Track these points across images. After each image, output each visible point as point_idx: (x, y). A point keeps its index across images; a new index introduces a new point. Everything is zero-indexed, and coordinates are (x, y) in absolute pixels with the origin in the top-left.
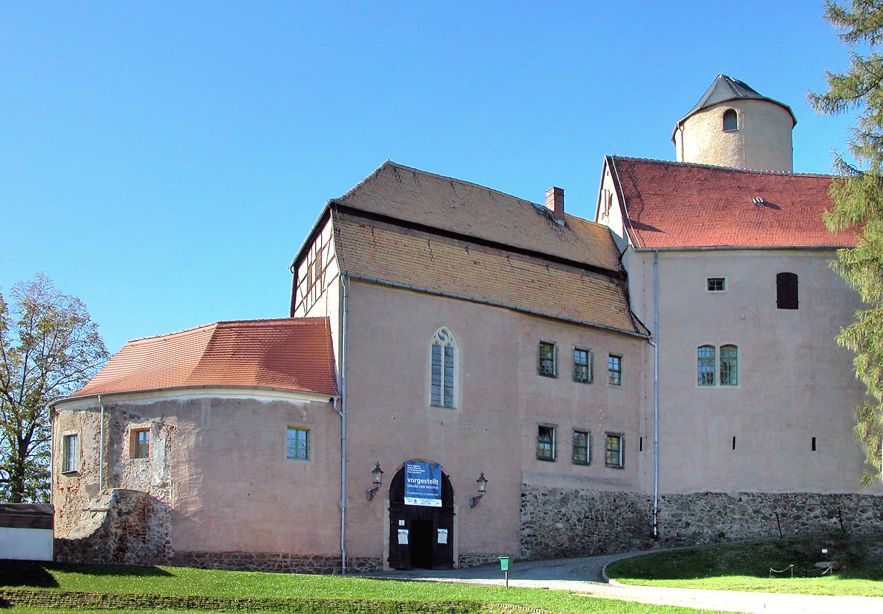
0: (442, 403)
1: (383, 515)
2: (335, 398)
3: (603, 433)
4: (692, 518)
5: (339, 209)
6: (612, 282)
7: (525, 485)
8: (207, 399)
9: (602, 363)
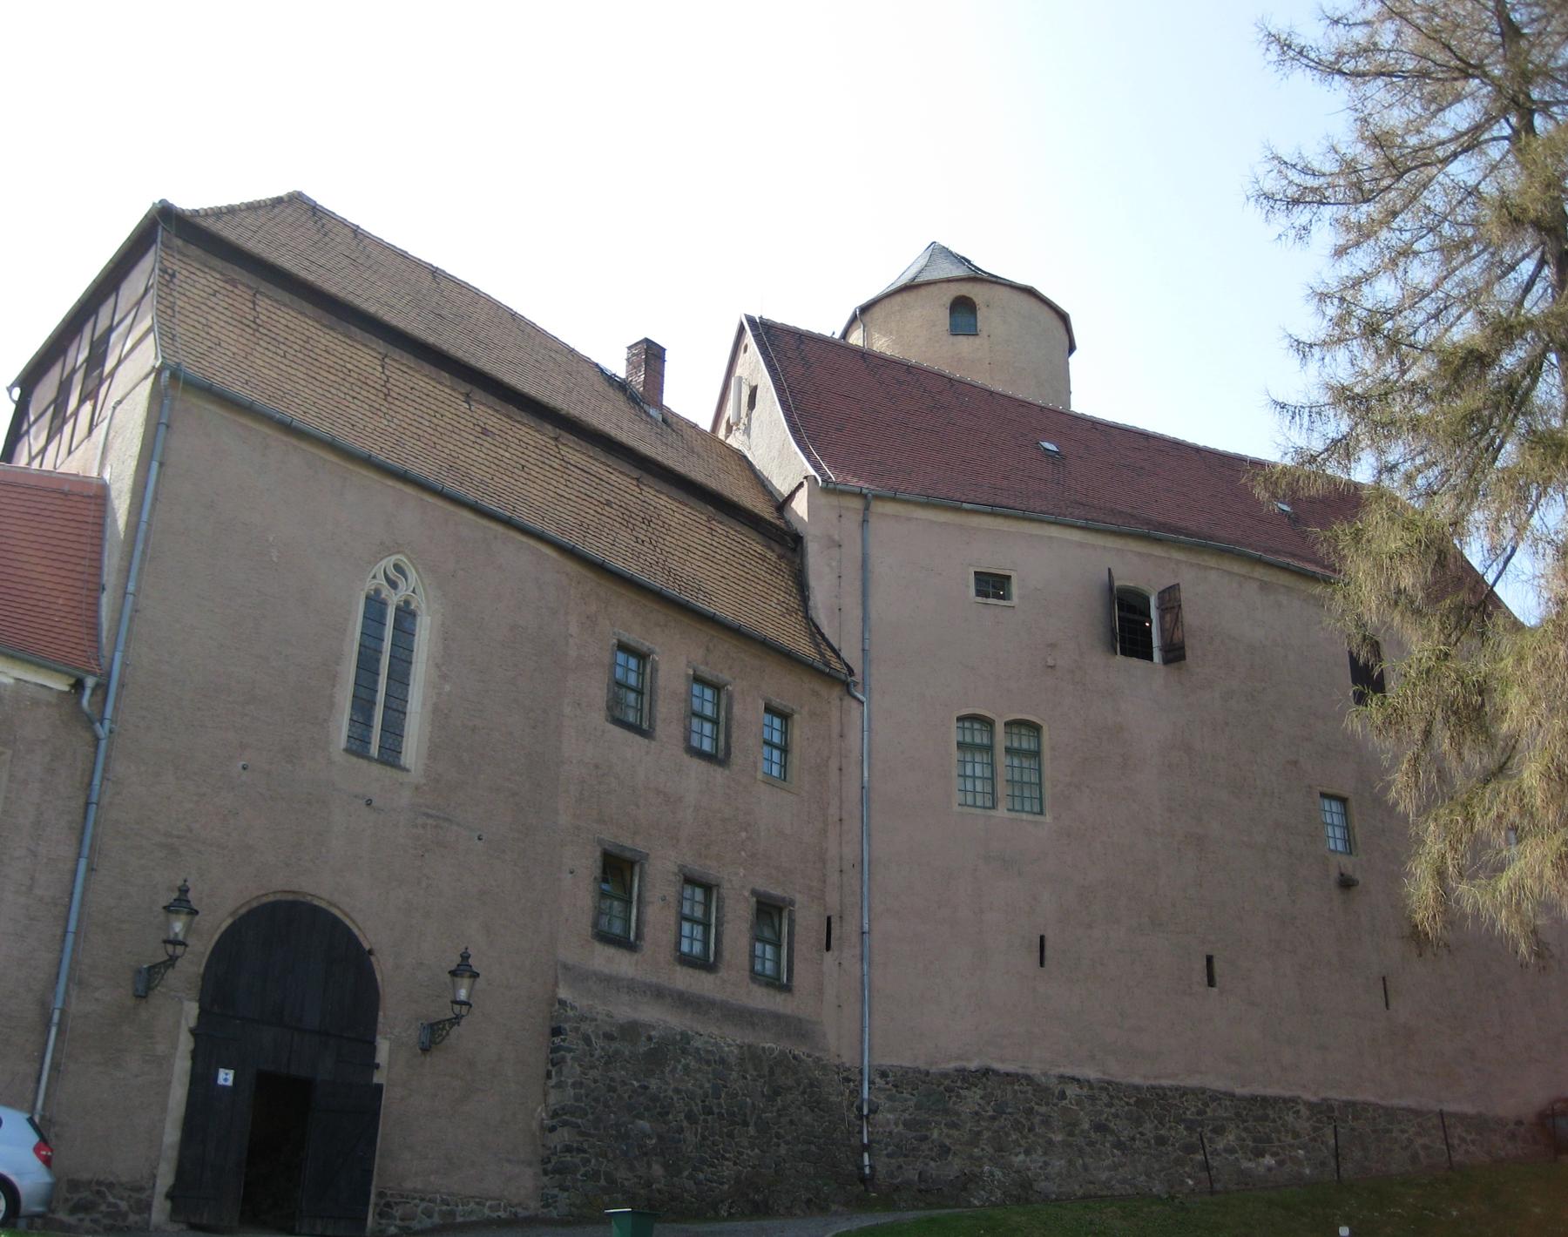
0: (374, 750)
1: (175, 1047)
2: (90, 682)
3: (747, 894)
4: (955, 1133)
6: (769, 548)
7: (562, 1003)
9: (749, 715)
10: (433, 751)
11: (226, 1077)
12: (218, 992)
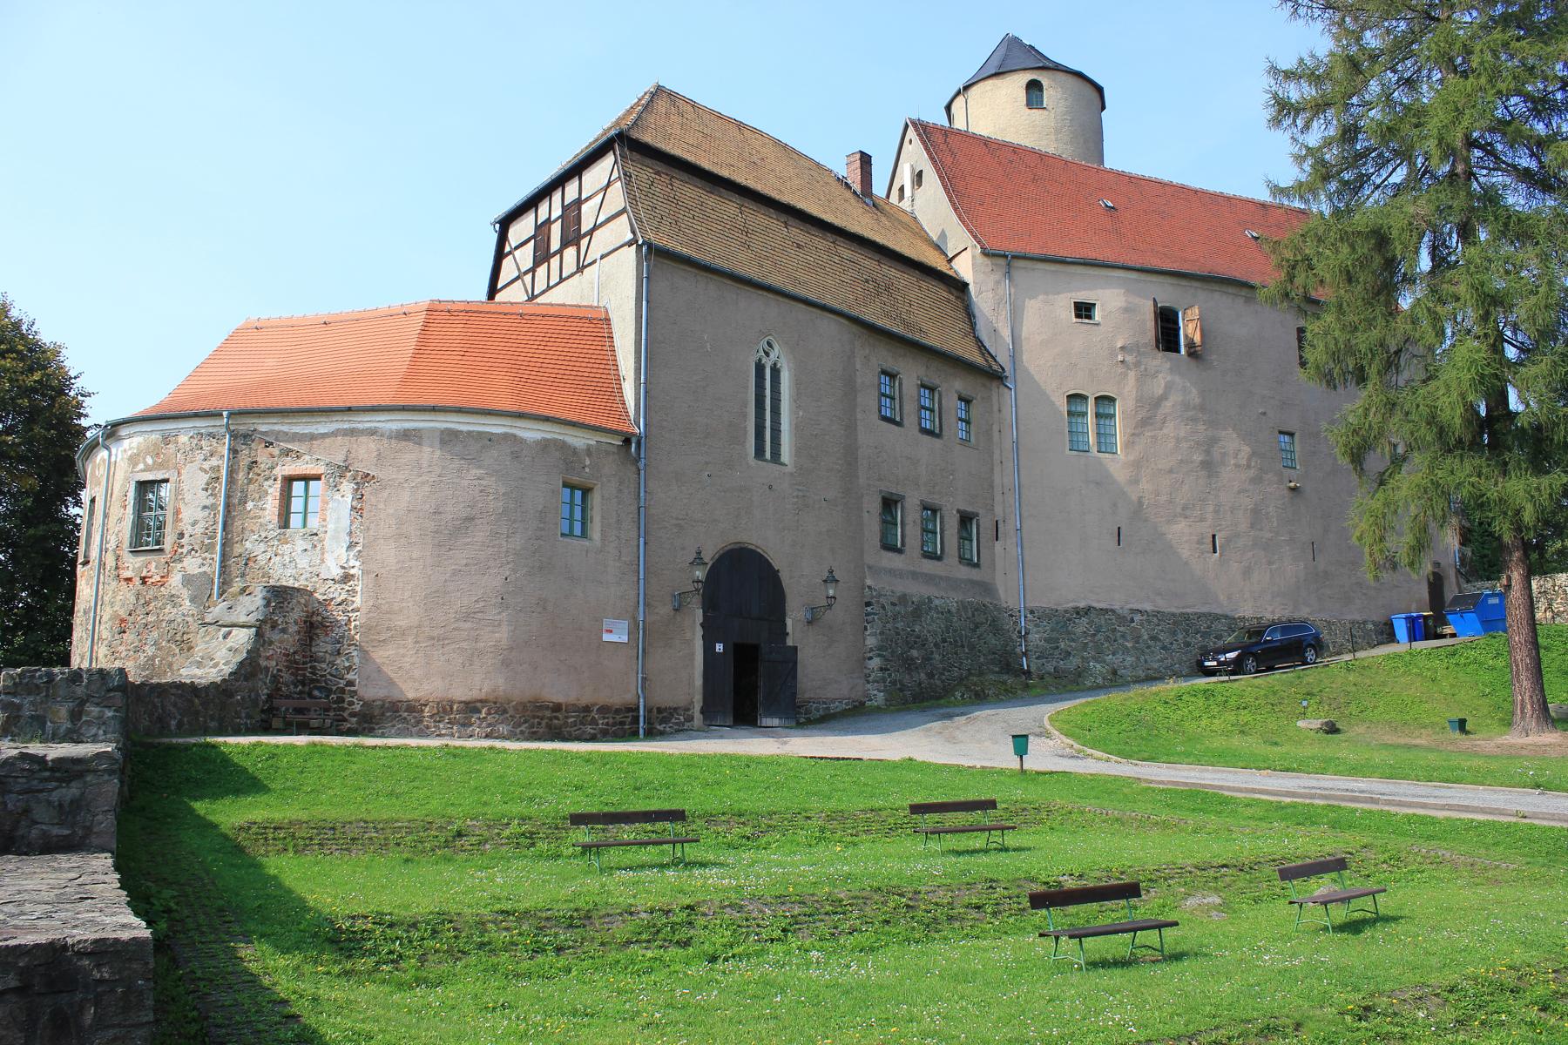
0: (768, 455)
8: (433, 430)
10: (798, 451)
11: (719, 647)
12: (710, 604)
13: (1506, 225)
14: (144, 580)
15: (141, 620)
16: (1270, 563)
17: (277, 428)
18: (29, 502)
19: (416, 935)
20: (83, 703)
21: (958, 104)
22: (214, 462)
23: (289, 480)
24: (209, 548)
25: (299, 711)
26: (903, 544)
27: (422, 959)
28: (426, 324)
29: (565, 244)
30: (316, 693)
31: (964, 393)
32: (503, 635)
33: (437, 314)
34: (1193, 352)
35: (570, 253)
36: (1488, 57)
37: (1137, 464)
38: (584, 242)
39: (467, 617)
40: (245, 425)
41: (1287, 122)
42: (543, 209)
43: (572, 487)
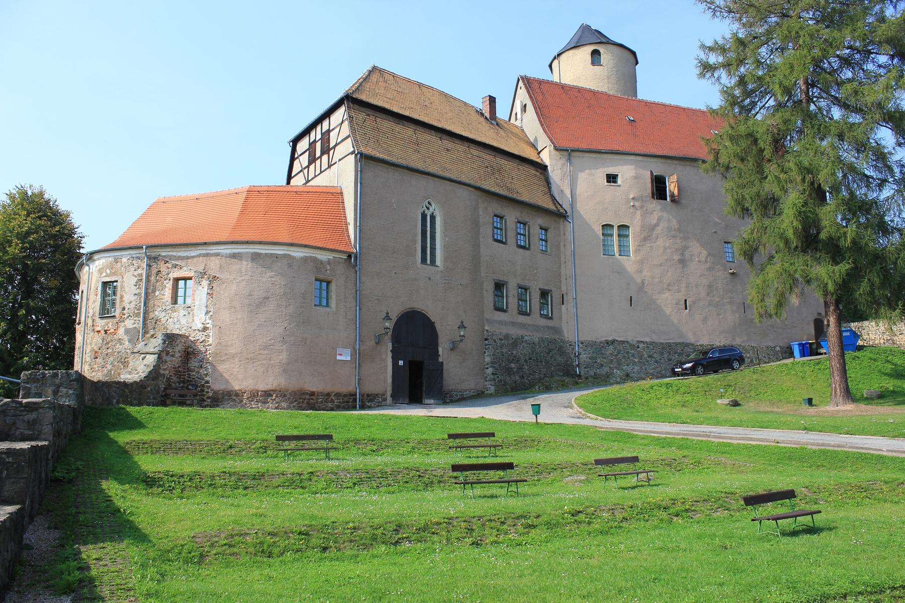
0: (429, 262)
5: (349, 100)
8: (248, 253)
9: (536, 231)
10: (446, 259)
11: (401, 363)
12: (396, 339)
13: (819, 129)
14: (106, 332)
15: (105, 351)
16: (718, 315)
17: (170, 253)
18: (54, 293)
19: (182, 480)
20: (58, 387)
21: (555, 64)
22: (140, 271)
23: (177, 280)
24: (138, 315)
25: (181, 396)
26: (507, 307)
27: (183, 490)
28: (247, 198)
29: (322, 153)
30: (190, 387)
31: (544, 225)
32: (284, 357)
33: (253, 193)
34: (673, 200)
35: (325, 157)
36: (808, 39)
37: (642, 262)
38: (331, 152)
39: (266, 348)
40: (154, 252)
41: (708, 75)
42: (313, 134)
43: (321, 281)
